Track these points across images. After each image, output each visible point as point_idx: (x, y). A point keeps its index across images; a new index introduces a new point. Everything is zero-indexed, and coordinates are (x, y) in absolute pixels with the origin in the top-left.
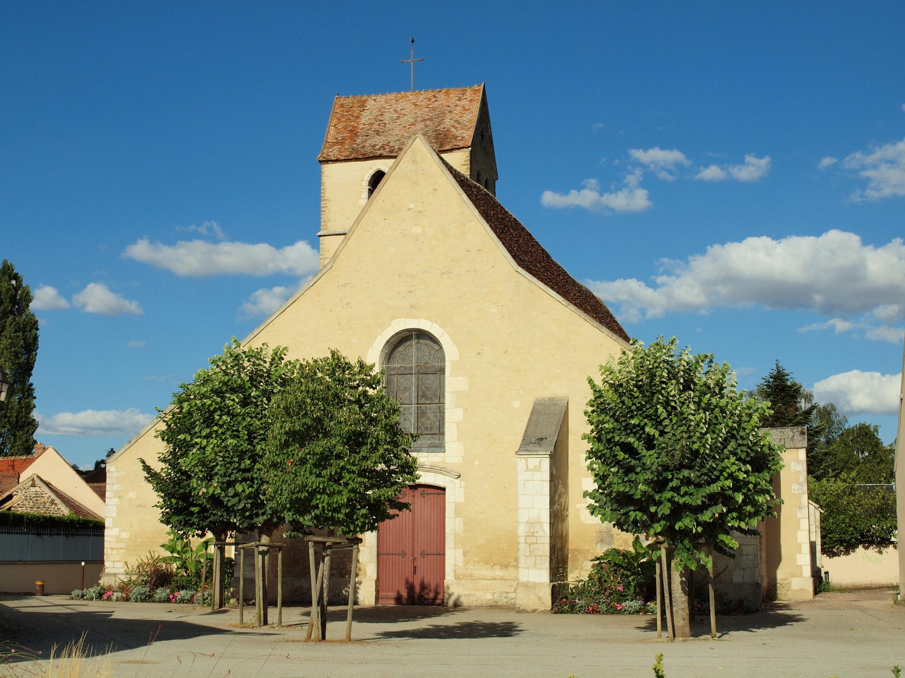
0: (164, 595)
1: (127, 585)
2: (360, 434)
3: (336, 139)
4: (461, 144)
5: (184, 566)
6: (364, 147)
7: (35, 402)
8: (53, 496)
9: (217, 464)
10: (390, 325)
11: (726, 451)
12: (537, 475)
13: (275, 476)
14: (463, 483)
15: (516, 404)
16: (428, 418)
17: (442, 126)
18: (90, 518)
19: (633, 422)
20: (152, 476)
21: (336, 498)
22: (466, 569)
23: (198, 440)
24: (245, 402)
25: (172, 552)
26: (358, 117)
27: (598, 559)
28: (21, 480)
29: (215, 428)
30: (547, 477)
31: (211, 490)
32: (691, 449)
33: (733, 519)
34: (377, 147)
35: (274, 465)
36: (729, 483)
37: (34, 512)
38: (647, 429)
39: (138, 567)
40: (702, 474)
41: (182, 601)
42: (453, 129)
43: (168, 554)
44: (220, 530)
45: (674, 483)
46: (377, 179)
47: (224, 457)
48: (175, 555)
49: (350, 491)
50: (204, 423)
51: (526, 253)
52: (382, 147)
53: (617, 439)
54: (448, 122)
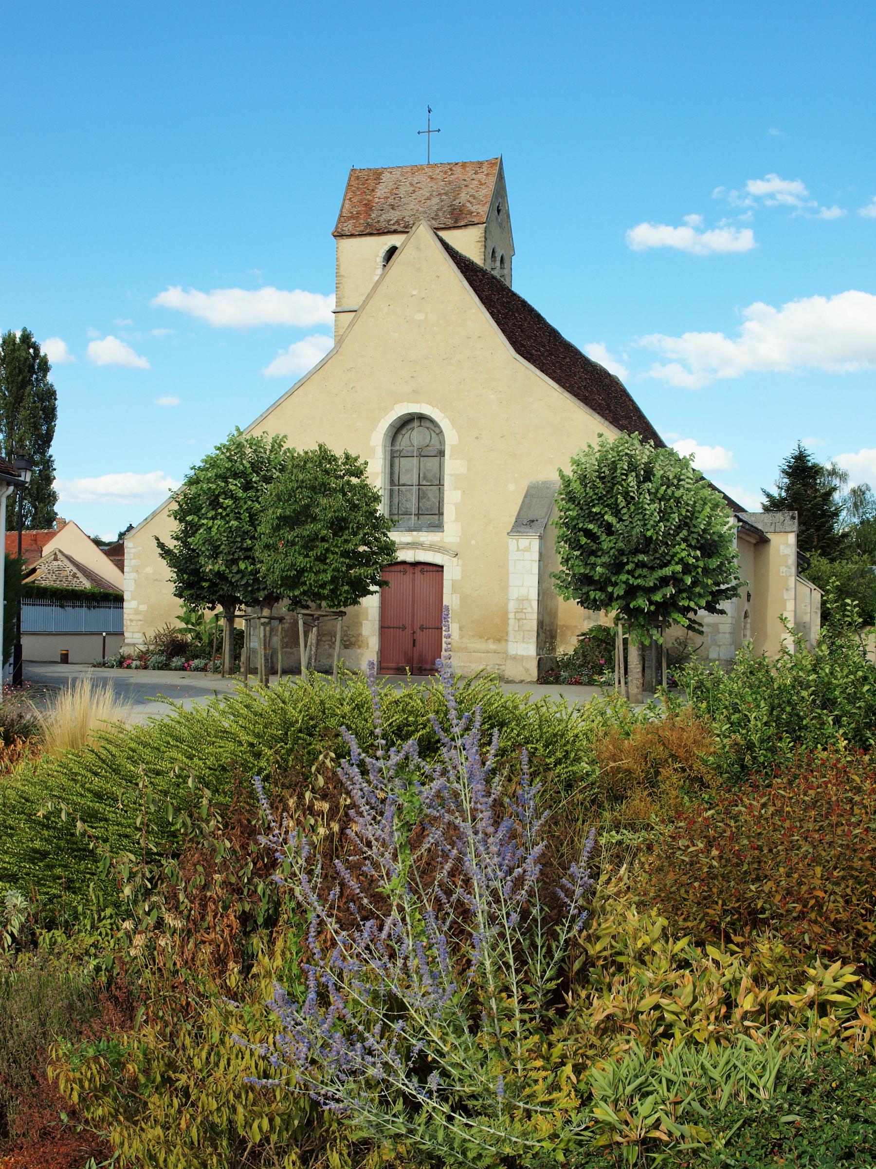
0: (179, 663)
1: (146, 654)
2: (344, 519)
3: (351, 213)
4: (476, 220)
5: (198, 636)
6: (378, 222)
7: (55, 473)
8: (75, 570)
9: (222, 543)
10: (392, 409)
11: (678, 538)
12: (527, 555)
13: (269, 556)
14: (460, 562)
15: (512, 487)
16: (428, 500)
17: (458, 201)
18: (111, 591)
19: (594, 510)
20: (166, 553)
21: (322, 576)
22: (462, 642)
23: (205, 521)
24: (248, 486)
25: (187, 624)
26: (373, 190)
27: (583, 634)
28: (44, 554)
29: (220, 511)
30: (536, 557)
31: (216, 568)
32: (645, 536)
33: (683, 599)
34: (392, 222)
35: (267, 547)
36: (679, 568)
37: (57, 585)
38: (606, 517)
39: (155, 638)
40: (655, 559)
41: (197, 669)
42: (468, 204)
43: (183, 625)
44: (230, 603)
45: (630, 567)
46: (392, 252)
47: (228, 537)
48: (190, 626)
49: (333, 570)
50: (210, 504)
51: (529, 337)
52: (397, 222)
53: (581, 525)
54: (463, 197)
